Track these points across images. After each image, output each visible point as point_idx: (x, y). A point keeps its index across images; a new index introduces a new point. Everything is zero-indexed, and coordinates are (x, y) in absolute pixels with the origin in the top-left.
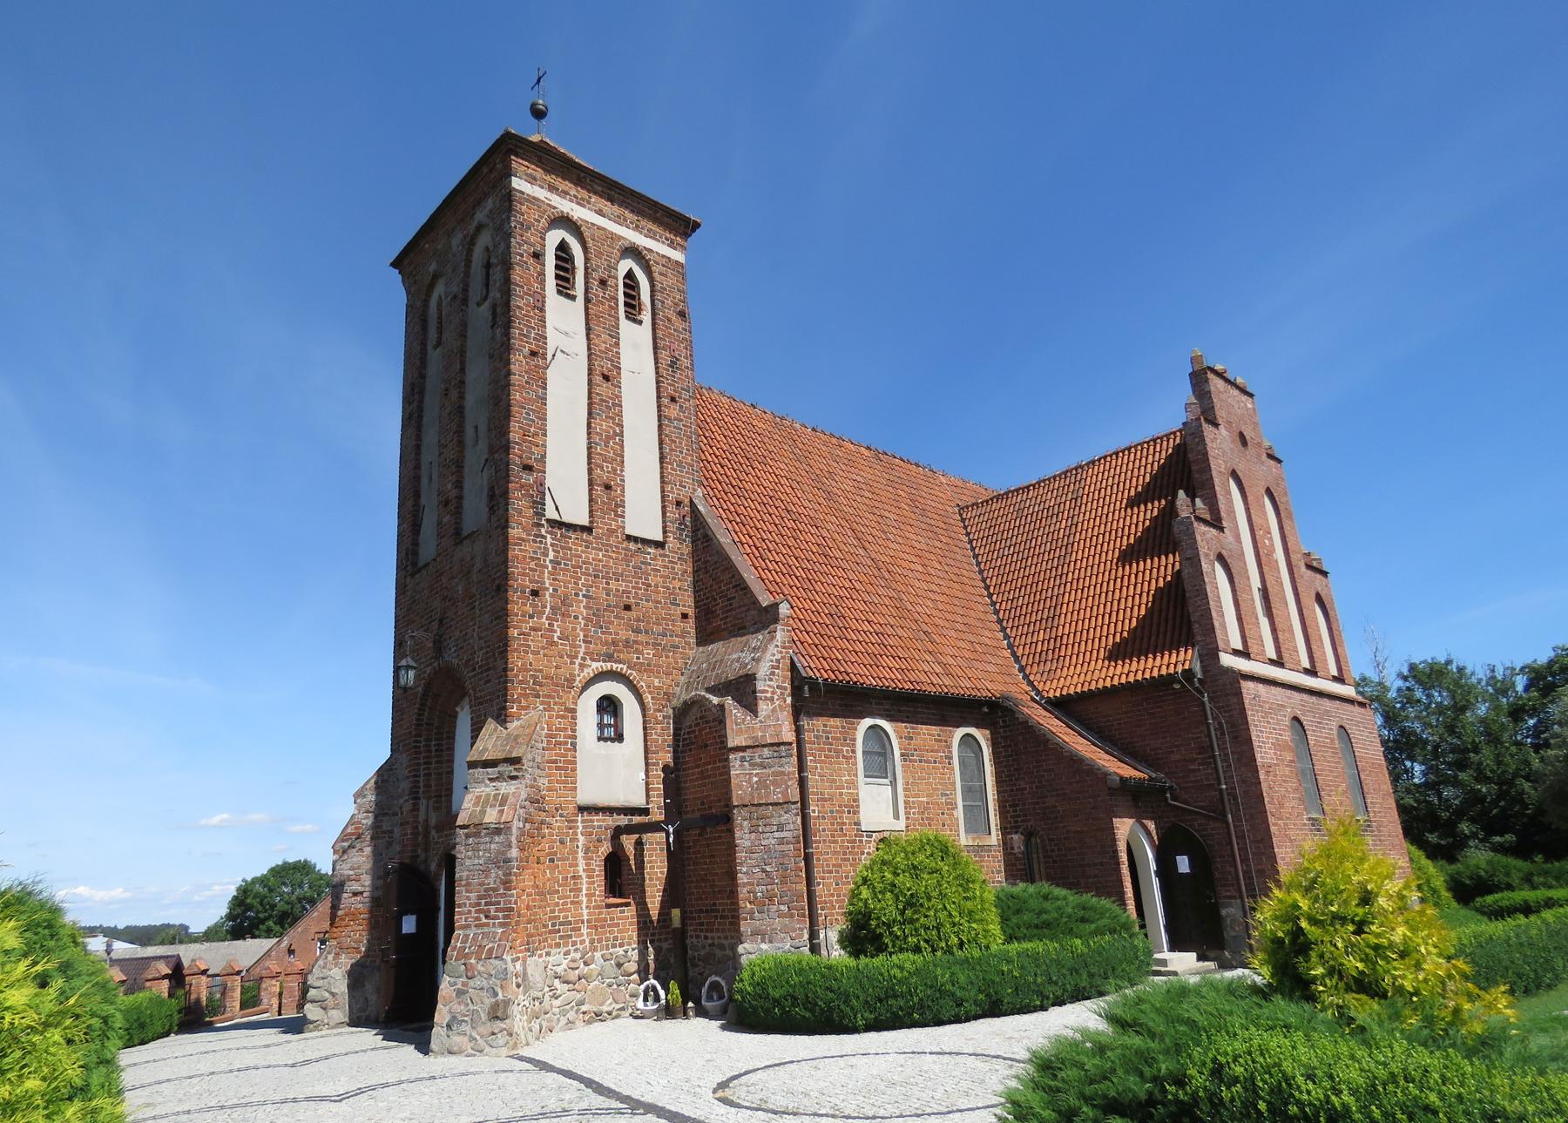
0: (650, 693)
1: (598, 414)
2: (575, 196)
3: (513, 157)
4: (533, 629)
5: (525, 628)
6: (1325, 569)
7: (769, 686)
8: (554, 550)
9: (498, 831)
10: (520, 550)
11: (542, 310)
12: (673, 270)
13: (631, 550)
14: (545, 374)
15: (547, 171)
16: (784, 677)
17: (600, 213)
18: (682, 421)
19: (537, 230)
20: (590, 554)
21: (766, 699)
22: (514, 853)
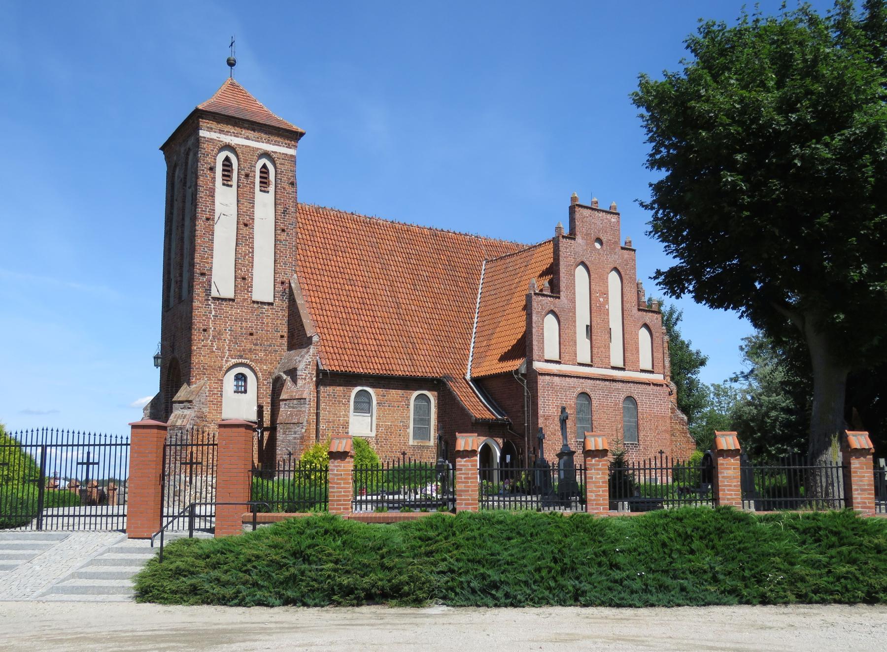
2: (233, 133)
4: (203, 346)
5: (200, 346)
11: (213, 196)
14: (213, 228)
15: (218, 122)
16: (313, 369)
17: (247, 138)
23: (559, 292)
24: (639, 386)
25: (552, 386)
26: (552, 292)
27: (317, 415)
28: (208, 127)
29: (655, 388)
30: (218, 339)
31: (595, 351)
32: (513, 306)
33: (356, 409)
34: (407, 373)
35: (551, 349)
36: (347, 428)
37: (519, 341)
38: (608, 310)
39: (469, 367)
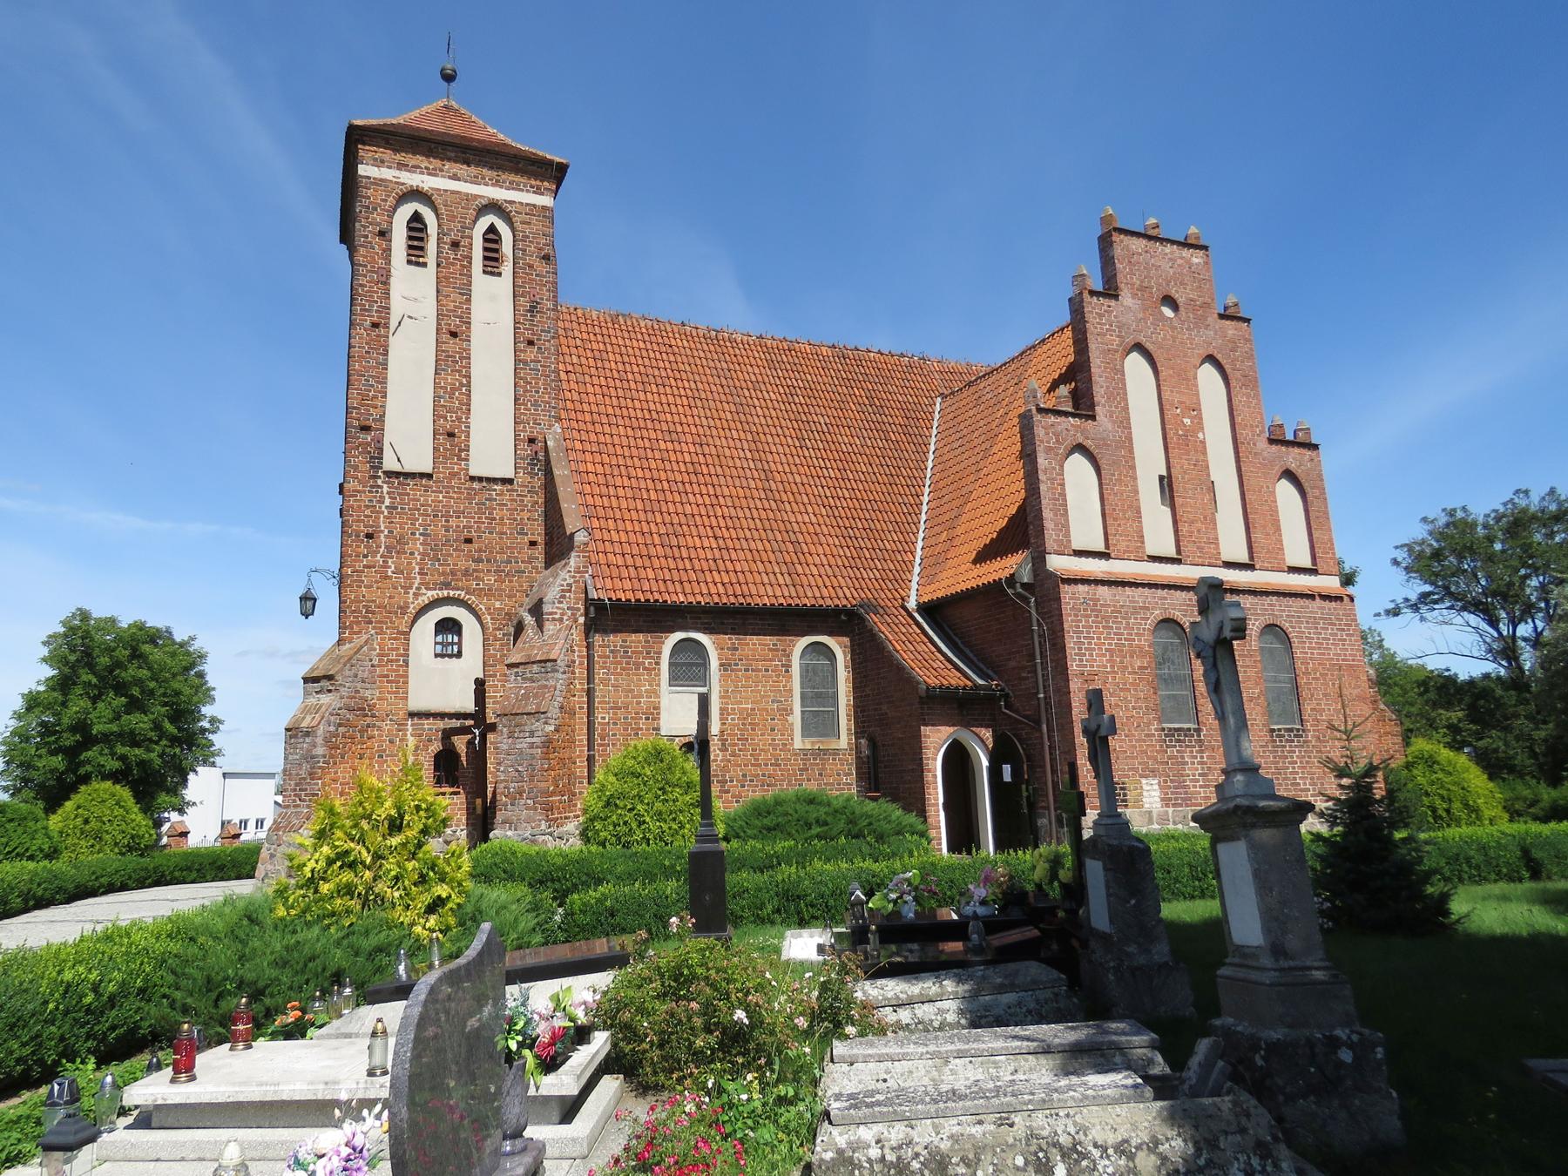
0: (489, 614)
1: (444, 370)
2: (426, 168)
3: (360, 146)
4: (365, 566)
6: (1314, 441)
7: (557, 608)
8: (390, 498)
9: (307, 734)
10: (355, 501)
11: (386, 283)
12: (539, 216)
13: (475, 489)
15: (396, 151)
16: (578, 599)
17: (455, 178)
18: (540, 361)
19: (384, 210)
20: (433, 497)
21: (554, 619)
22: (320, 751)
23: (1092, 406)
24: (1291, 601)
25: (1094, 605)
26: (1076, 405)
27: (590, 693)
28: (375, 160)
29: (1327, 604)
30: (398, 552)
31: (1184, 529)
32: (996, 458)
33: (675, 680)
34: (781, 600)
35: (1085, 526)
36: (657, 718)
37: (1012, 519)
38: (1203, 442)
39: (914, 585)
